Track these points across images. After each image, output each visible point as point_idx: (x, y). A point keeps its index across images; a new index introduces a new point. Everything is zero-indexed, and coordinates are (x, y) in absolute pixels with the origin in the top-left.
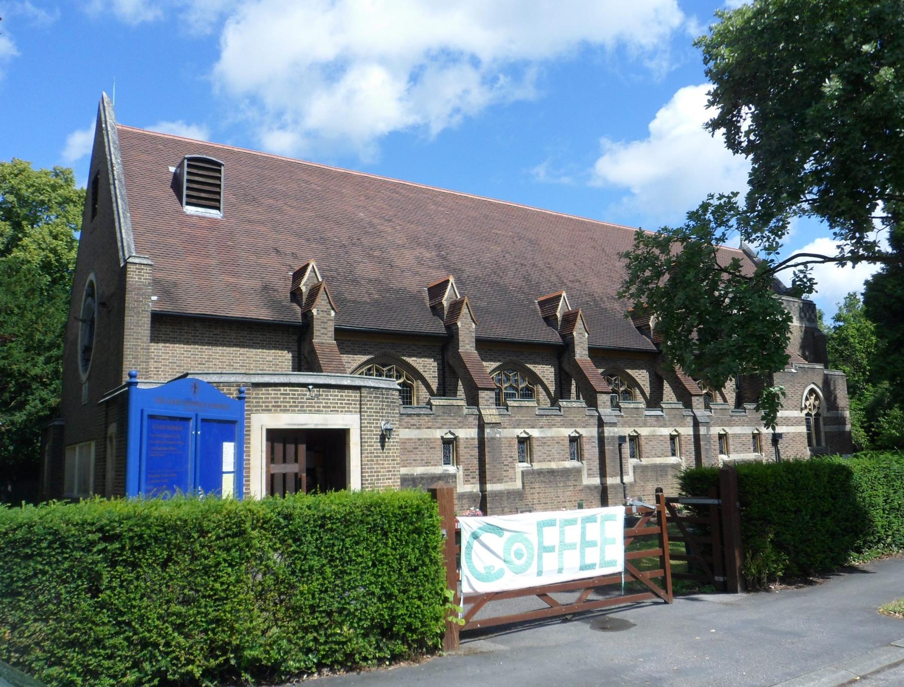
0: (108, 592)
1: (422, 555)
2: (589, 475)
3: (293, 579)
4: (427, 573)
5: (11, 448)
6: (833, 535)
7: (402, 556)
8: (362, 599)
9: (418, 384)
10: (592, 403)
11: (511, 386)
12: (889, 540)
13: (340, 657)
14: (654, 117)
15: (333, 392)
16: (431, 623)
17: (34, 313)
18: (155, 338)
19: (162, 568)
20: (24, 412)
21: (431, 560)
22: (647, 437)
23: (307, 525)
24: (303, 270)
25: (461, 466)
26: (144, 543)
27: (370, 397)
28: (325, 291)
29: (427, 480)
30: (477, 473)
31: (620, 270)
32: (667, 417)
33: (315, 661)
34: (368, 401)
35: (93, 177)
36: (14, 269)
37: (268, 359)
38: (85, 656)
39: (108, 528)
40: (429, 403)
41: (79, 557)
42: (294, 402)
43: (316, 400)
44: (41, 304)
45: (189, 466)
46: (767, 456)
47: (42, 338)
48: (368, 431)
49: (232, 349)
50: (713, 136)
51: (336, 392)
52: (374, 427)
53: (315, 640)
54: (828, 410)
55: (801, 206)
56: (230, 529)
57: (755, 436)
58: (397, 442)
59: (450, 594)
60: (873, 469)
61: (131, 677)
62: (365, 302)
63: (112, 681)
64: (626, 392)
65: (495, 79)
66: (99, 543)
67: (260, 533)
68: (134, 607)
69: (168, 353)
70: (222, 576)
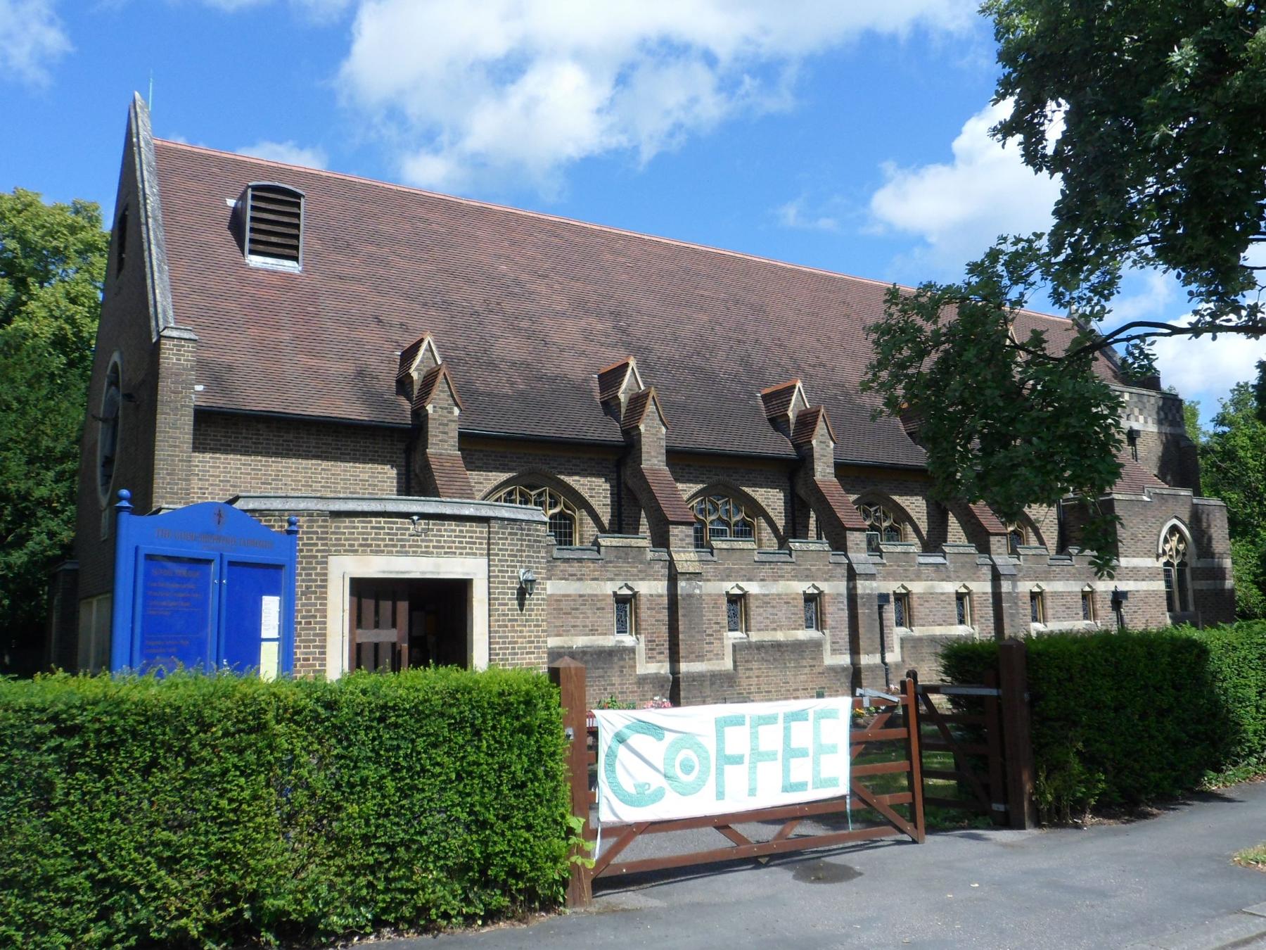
0: (63, 809)
1: (532, 764)
2: (834, 651)
3: (337, 797)
7: (503, 767)
9: (581, 516)
10: (839, 544)
11: (720, 519)
13: (406, 911)
15: (449, 525)
16: (545, 866)
17: (40, 410)
18: (200, 445)
19: (143, 776)
20: (25, 551)
23: (359, 718)
24: (415, 348)
25: (643, 636)
26: (115, 739)
27: (503, 533)
28: (446, 379)
29: (592, 655)
30: (667, 645)
31: (866, 351)
33: (369, 916)
34: (500, 539)
35: (119, 216)
36: (14, 346)
39: (64, 716)
40: (596, 543)
41: (20, 757)
42: (391, 540)
43: (423, 537)
45: (209, 630)
46: (1104, 621)
47: (51, 445)
49: (310, 462)
51: (453, 525)
52: (509, 577)
53: (370, 885)
55: (1142, 251)
56: (244, 721)
57: (1085, 596)
58: (543, 599)
59: (576, 823)
60: (1240, 647)
61: (95, 934)
62: (506, 396)
63: (67, 939)
64: (891, 528)
66: (52, 737)
67: (289, 728)
68: (102, 832)
69: (219, 467)
70: (231, 790)
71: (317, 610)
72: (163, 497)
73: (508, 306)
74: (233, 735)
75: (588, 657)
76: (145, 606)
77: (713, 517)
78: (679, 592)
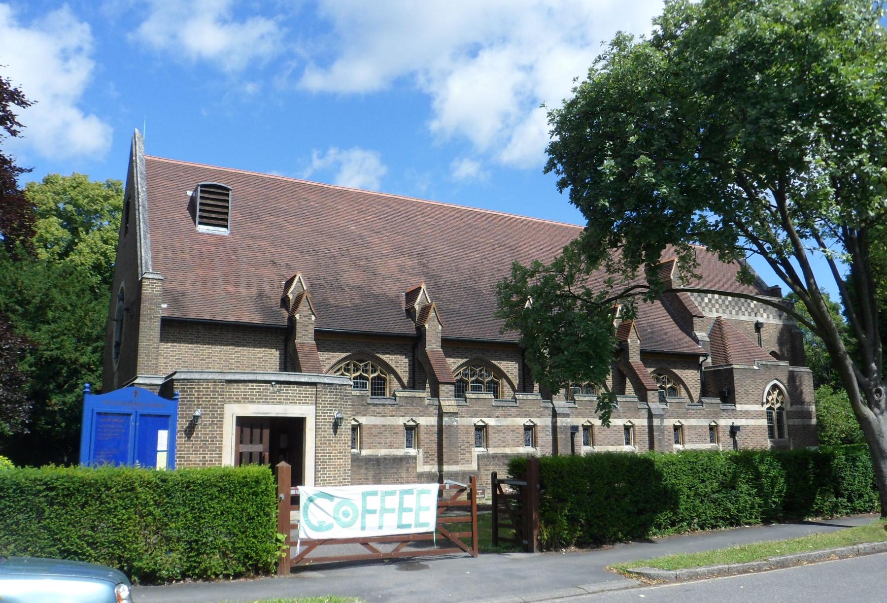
0: (48, 520)
3: (166, 519)
5: (63, 424)
7: (243, 510)
9: (390, 378)
21: (265, 514)
37: (259, 356)
42: (259, 395)
46: (724, 445)
48: (322, 419)
49: (228, 348)
57: (712, 428)
62: (348, 307)
68: (64, 530)
71: (217, 434)
72: (142, 369)
74: (120, 492)
75: (387, 461)
76: (96, 435)
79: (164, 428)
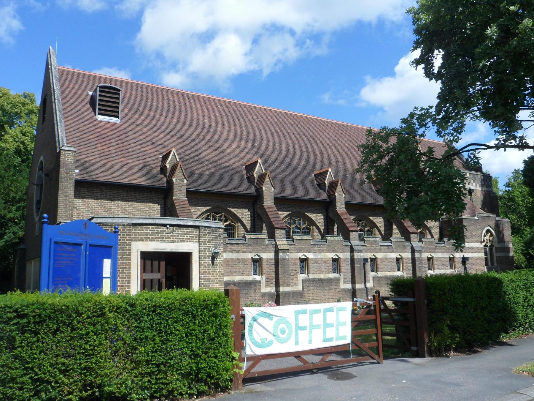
0: (19, 349)
1: (217, 330)
2: (345, 282)
3: (135, 344)
4: (220, 342)
6: (489, 321)
7: (205, 331)
8: (179, 357)
9: (238, 225)
10: (347, 237)
11: (296, 227)
12: (527, 325)
13: (164, 392)
14: (397, 64)
15: (182, 229)
17: (10, 180)
19: (53, 335)
20: (4, 240)
22: (382, 259)
23: (144, 311)
24: (168, 154)
25: (264, 276)
26: (41, 320)
27: (205, 233)
28: (181, 167)
29: (242, 284)
30: (274, 280)
32: (394, 247)
33: (149, 394)
34: (204, 235)
35: (44, 97)
37: (146, 209)
38: (5, 388)
40: (244, 237)
44: (14, 175)
46: (459, 270)
47: (15, 196)
48: (203, 253)
49: (124, 203)
50: (416, 69)
52: (208, 251)
53: (149, 381)
54: (499, 242)
55: (475, 114)
56: (96, 312)
58: (222, 261)
59: (236, 355)
64: (369, 231)
65: (304, 43)
66: (15, 319)
67: (115, 315)
68: (36, 359)
69: (85, 205)
71: (126, 265)
72: (62, 218)
73: (207, 137)
74: (91, 318)
75: (241, 285)
77: (294, 226)
78: (279, 257)
79: (108, 257)
